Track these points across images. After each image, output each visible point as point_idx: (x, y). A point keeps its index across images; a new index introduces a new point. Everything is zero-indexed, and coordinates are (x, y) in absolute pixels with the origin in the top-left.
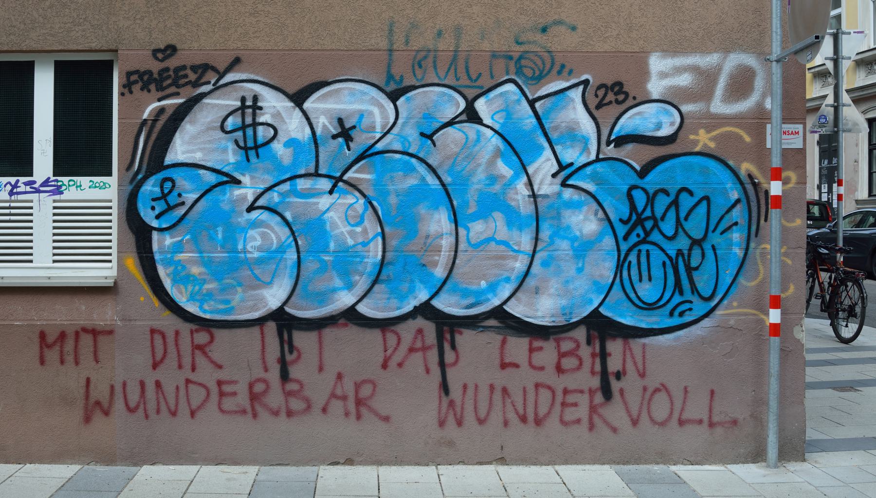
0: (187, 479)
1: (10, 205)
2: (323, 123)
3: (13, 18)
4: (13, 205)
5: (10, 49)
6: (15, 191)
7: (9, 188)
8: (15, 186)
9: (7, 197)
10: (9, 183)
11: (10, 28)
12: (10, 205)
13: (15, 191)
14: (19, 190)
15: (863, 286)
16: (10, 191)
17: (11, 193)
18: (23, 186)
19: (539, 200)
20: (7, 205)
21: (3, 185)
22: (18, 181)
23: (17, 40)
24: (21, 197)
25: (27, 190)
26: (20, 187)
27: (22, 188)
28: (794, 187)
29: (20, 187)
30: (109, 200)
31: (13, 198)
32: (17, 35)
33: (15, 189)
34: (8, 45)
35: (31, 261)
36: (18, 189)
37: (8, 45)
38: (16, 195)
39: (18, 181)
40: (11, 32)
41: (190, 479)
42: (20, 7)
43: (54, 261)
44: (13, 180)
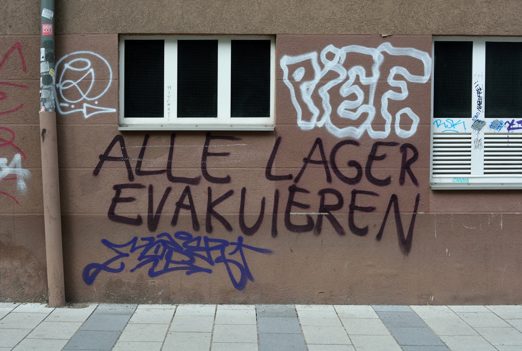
0: (29, 328)
1: (508, 136)
2: (90, 73)
3: (515, 14)
4: (510, 136)
5: (514, 35)
6: (511, 127)
7: (507, 125)
8: (512, 124)
9: (507, 131)
10: (508, 122)
11: (514, 21)
12: (508, 136)
13: (511, 127)
14: (514, 126)
15: (49, 294)
16: (508, 127)
17: (509, 129)
18: (517, 124)
19: (141, 140)
20: (506, 136)
21: (504, 123)
22: (513, 121)
23: (519, 28)
24: (515, 131)
25: (519, 127)
26: (515, 124)
27: (516, 125)
28: (120, 136)
29: (515, 124)
30: (469, 133)
31: (510, 131)
32: (519, 25)
33: (512, 126)
34: (513, 31)
35: (470, 173)
36: (513, 126)
37: (513, 31)
38: (512, 130)
39: (513, 121)
40: (515, 23)
41: (31, 328)
42: (520, 7)
43: (485, 173)
44: (510, 120)
